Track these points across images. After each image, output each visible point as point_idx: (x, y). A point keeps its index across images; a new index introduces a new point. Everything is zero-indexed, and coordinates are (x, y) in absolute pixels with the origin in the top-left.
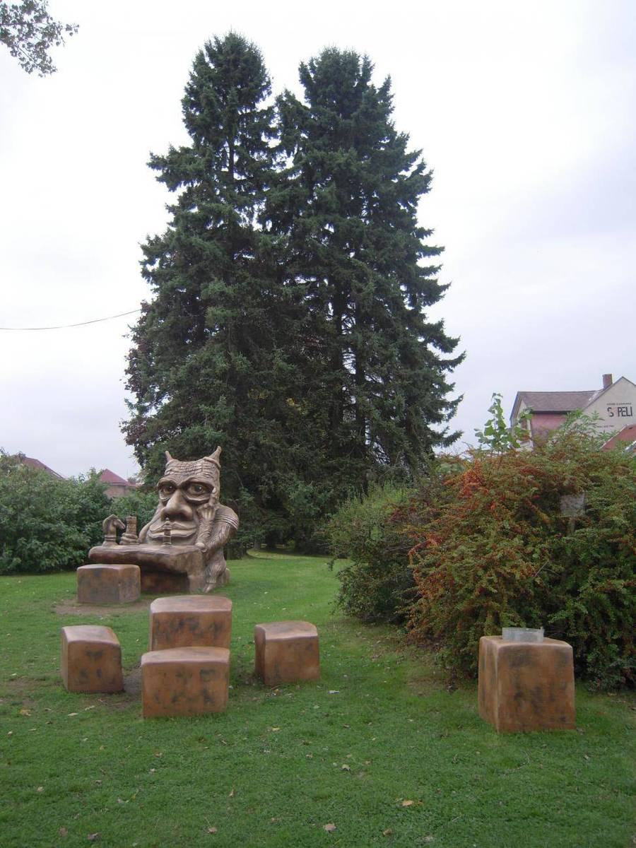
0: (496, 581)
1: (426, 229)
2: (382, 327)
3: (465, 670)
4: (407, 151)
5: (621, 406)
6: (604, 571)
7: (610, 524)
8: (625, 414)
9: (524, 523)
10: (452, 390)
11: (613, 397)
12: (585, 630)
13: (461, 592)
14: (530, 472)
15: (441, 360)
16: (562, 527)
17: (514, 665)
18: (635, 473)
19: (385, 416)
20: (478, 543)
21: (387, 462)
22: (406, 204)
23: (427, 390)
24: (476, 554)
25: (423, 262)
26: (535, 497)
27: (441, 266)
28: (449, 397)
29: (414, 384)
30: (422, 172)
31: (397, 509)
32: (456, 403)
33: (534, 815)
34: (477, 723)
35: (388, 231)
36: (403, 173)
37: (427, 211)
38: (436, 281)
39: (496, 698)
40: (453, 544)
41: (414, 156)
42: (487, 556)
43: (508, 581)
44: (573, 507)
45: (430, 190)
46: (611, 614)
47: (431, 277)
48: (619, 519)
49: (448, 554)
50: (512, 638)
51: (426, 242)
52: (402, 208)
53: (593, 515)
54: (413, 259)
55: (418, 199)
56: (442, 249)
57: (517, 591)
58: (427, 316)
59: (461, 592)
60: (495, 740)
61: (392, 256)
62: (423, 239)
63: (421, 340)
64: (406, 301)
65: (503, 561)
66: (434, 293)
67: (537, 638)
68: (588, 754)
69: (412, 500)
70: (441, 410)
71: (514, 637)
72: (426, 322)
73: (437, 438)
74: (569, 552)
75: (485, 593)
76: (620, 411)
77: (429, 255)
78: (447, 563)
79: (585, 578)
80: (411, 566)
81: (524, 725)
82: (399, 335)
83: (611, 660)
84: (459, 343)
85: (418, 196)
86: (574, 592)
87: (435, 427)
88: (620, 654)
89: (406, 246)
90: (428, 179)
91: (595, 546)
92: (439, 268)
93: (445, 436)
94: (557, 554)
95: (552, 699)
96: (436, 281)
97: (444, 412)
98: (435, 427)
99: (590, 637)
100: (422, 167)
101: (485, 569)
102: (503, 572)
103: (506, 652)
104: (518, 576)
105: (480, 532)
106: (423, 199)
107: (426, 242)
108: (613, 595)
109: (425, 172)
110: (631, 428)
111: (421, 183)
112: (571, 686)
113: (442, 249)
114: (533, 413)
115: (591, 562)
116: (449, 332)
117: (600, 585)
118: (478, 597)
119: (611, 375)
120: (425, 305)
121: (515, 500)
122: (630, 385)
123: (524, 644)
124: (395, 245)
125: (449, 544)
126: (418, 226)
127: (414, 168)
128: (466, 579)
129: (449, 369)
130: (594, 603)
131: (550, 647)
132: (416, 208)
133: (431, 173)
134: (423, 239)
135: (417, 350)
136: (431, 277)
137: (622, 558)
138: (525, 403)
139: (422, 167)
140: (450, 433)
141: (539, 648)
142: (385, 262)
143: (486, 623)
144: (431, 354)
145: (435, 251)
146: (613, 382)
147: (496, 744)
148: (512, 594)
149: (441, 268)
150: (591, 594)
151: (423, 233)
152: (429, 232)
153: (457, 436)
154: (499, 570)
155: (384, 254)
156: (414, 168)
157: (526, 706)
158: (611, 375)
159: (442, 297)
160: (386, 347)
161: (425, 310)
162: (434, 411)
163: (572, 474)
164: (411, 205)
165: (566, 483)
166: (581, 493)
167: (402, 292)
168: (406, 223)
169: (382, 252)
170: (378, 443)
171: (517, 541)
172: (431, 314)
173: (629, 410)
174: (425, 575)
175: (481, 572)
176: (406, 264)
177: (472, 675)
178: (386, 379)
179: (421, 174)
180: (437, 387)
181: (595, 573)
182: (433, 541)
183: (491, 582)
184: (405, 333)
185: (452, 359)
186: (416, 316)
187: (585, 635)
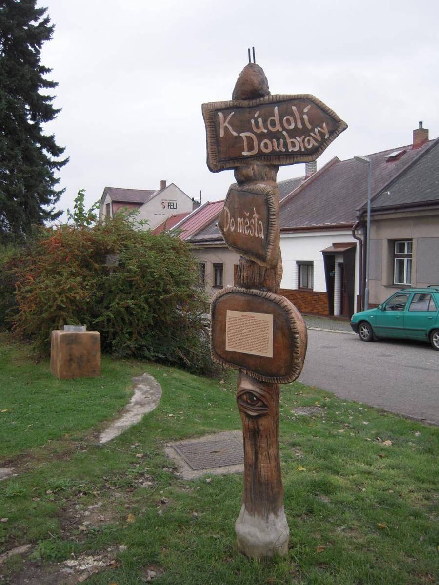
0: (65, 301)
1: (47, 67)
2: (10, 134)
3: (45, 352)
4: (37, 7)
5: (170, 202)
6: (124, 296)
7: (129, 271)
8: (172, 207)
9: (85, 269)
10: (59, 183)
11: (167, 195)
12: (112, 328)
13: (45, 307)
14: (90, 240)
15: (52, 161)
16: (105, 272)
17: (68, 344)
18: (416, 277)
19: (10, 198)
20: (56, 280)
21: (10, 230)
22: (33, 46)
23: (41, 182)
24: (55, 286)
25: (42, 91)
26: (91, 254)
27: (55, 96)
28: (56, 188)
29: (31, 177)
30: (47, 25)
31: (11, 260)
32: (61, 192)
33: (68, 409)
34: (48, 377)
35: (18, 65)
36: (32, 23)
37: (48, 54)
38: (51, 106)
39: (58, 362)
40: (42, 280)
41: (42, 11)
42: (61, 287)
43: (72, 301)
44: (112, 261)
45: (51, 39)
46: (126, 318)
47: (48, 103)
48: (134, 268)
49: (39, 285)
50: (69, 330)
51: (45, 77)
52: (30, 48)
53: (122, 265)
54: (35, 88)
55: (42, 44)
56: (56, 84)
57: (77, 306)
58: (43, 129)
59: (45, 307)
60: (57, 383)
61: (20, 84)
62: (44, 74)
63: (38, 145)
64: (29, 117)
65: (70, 289)
66: (49, 114)
67: (83, 330)
68: (103, 386)
69: (22, 255)
70: (50, 196)
71: (70, 330)
72: (42, 134)
73: (47, 215)
74: (107, 285)
75: (60, 308)
76: (169, 204)
77: (47, 87)
78: (38, 290)
79: (114, 299)
80: (16, 292)
81: (73, 375)
82: (22, 141)
83: (125, 343)
84: (65, 151)
85: (43, 42)
86: (107, 308)
87: (44, 207)
88: (130, 340)
89: (31, 78)
90: (50, 30)
91: (120, 282)
92: (54, 97)
93: (52, 213)
94: (101, 287)
95: (88, 361)
96: (51, 106)
97: (52, 198)
98: (44, 207)
99: (115, 331)
100: (47, 21)
101: (60, 294)
102: (70, 296)
103: (64, 337)
104: (78, 298)
105: (58, 273)
106: (46, 45)
107: (45, 77)
108: (127, 308)
109: (49, 25)
110: (175, 217)
111: (45, 33)
112: (99, 354)
113: (56, 84)
114: (114, 202)
115: (118, 291)
116: (58, 143)
117: (121, 303)
118: (55, 310)
119: (165, 181)
120: (42, 121)
121: (80, 256)
122: (177, 189)
123: (74, 332)
124: (23, 76)
125: (39, 279)
126: (41, 64)
127: (41, 20)
128: (48, 300)
129: (57, 168)
130: (118, 313)
131: (88, 334)
132: (40, 50)
133: (53, 26)
134: (44, 74)
135: (35, 154)
136: (48, 103)
137: (134, 289)
138: (110, 196)
139: (47, 21)
140: (55, 211)
141: (82, 334)
142: (14, 88)
143: (60, 324)
144: (45, 156)
145: (52, 85)
146: (167, 186)
147: (57, 385)
148: (74, 307)
149: (56, 98)
150: (117, 308)
151: (44, 70)
152: (48, 70)
153: (60, 213)
154: (67, 295)
155: (14, 81)
156: (41, 20)
157: (74, 365)
158: (165, 181)
159: (55, 118)
160: (12, 149)
161: (42, 125)
162: (45, 196)
163: (113, 243)
164: (37, 47)
165: (108, 247)
166: (118, 253)
167: (26, 109)
168: (33, 60)
169: (13, 79)
170: (4, 215)
171: (79, 279)
172: (47, 129)
173: (175, 205)
174: (24, 298)
175: (57, 296)
176: (30, 92)
177: (48, 355)
178: (12, 171)
179: (45, 26)
180: (48, 179)
181: (120, 297)
182: (30, 278)
183: (62, 301)
184: (27, 140)
185: (60, 161)
186: (37, 129)
187: (112, 330)
